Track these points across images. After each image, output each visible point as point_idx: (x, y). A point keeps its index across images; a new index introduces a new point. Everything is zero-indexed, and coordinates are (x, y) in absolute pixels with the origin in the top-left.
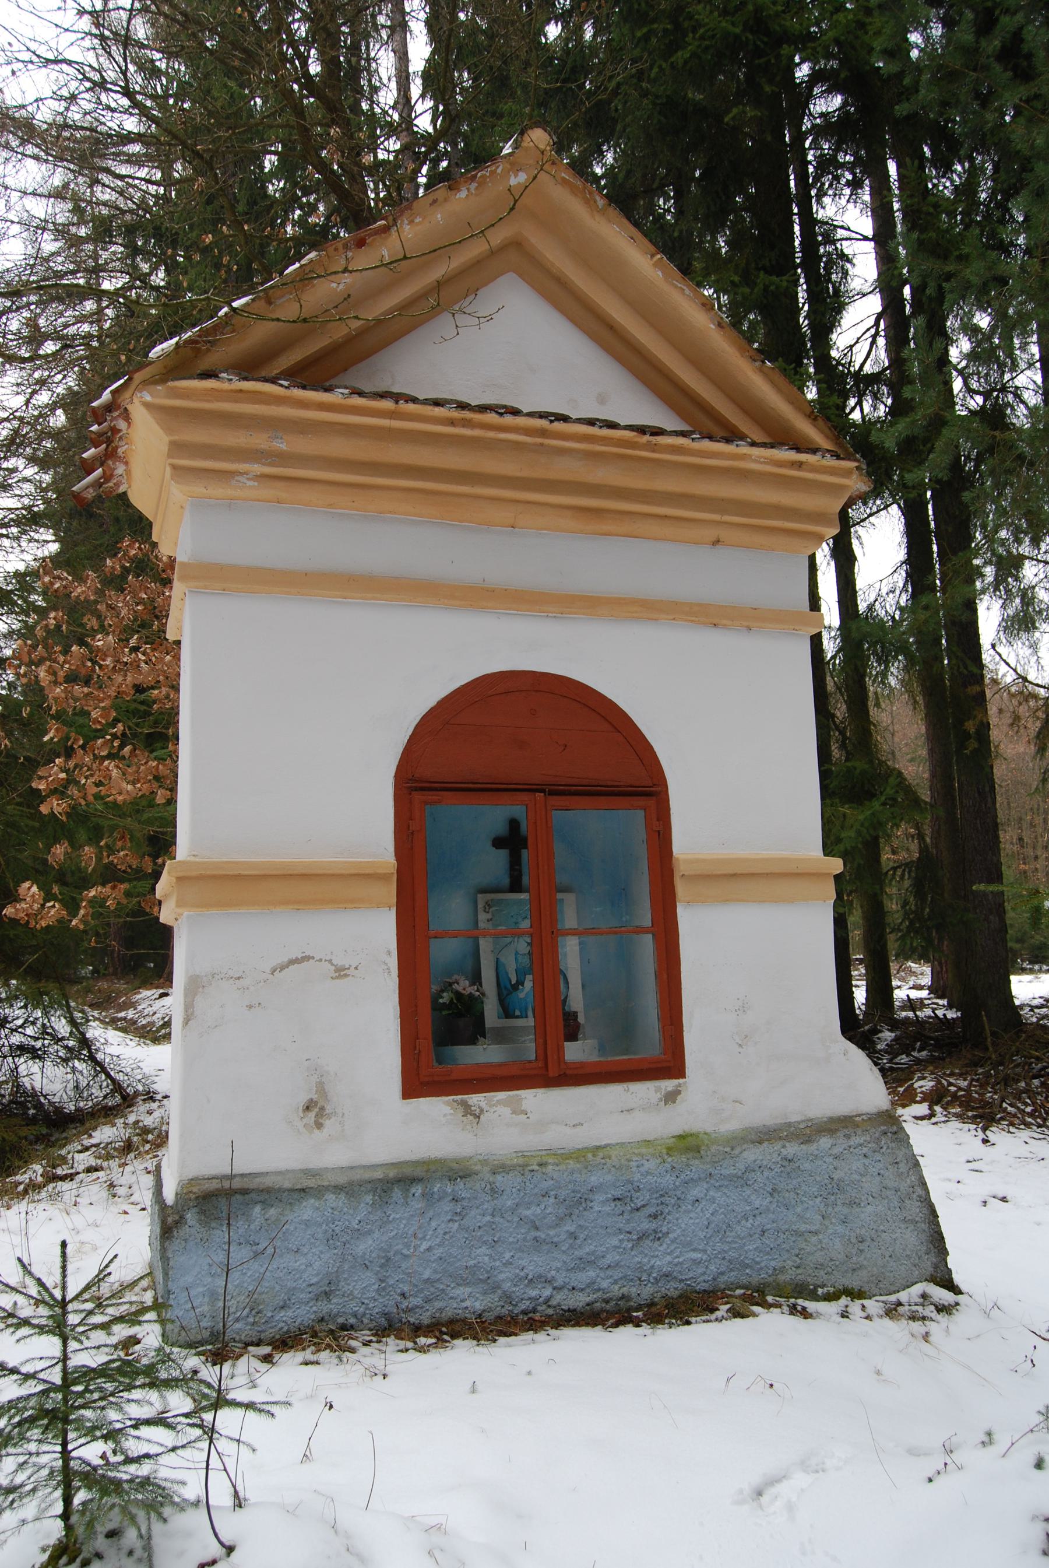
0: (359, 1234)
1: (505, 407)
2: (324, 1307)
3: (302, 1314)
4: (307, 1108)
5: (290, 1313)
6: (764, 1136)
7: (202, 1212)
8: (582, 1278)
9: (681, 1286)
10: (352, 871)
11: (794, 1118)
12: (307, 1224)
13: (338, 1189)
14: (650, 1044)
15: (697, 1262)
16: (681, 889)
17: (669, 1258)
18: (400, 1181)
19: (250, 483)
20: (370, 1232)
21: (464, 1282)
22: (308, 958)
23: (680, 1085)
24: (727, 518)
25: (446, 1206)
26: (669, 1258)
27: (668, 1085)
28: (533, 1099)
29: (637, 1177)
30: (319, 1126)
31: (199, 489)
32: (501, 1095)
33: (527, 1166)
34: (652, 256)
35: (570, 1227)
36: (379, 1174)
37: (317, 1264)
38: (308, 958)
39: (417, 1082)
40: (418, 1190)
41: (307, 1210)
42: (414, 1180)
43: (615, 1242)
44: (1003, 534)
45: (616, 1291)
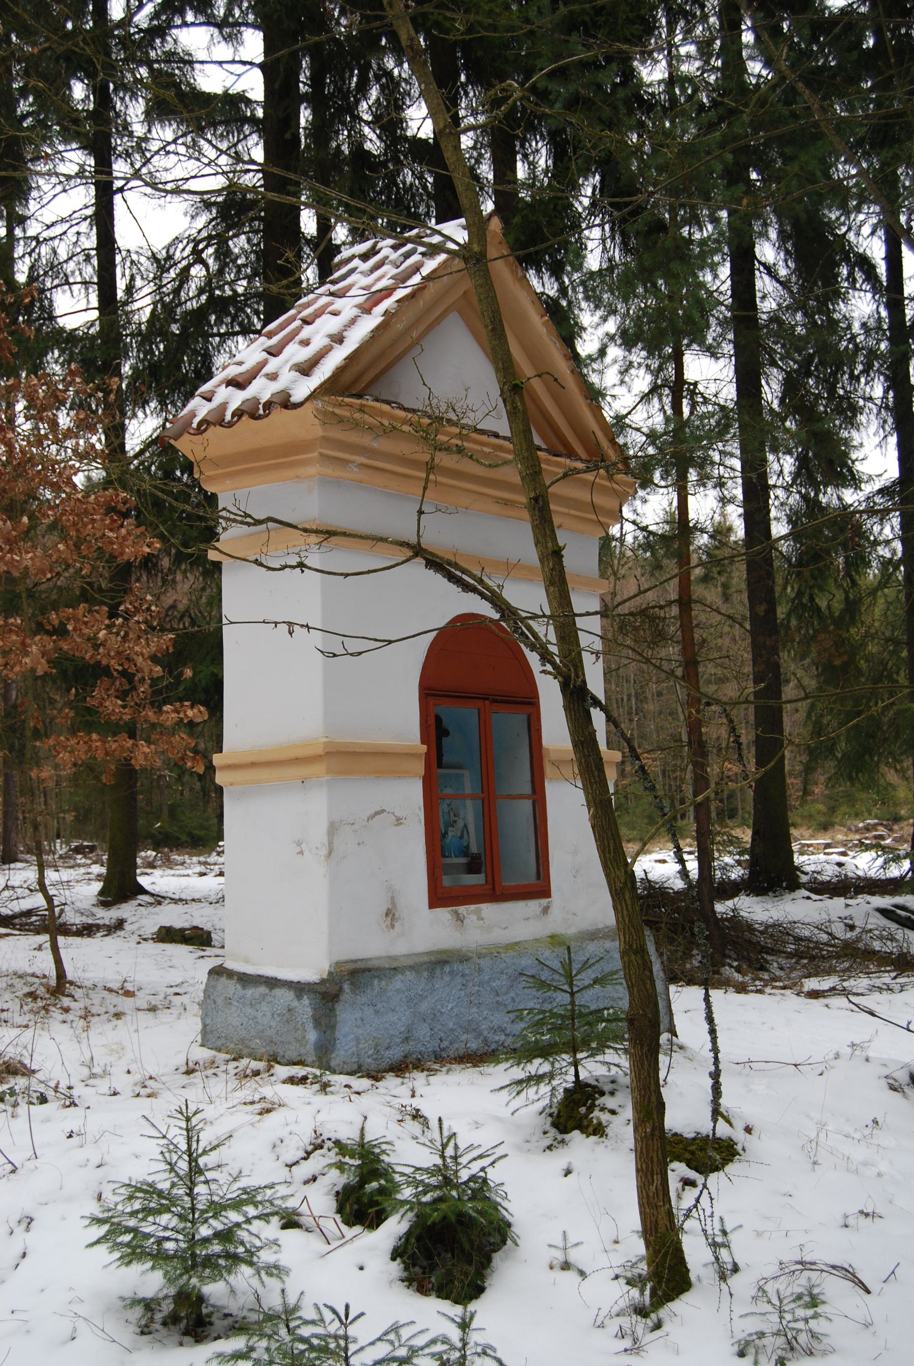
0: (422, 997)
2: (407, 1048)
3: (395, 1054)
4: (387, 915)
7: (352, 984)
11: (601, 926)
12: (398, 991)
13: (411, 968)
16: (549, 770)
18: (439, 963)
19: (355, 469)
20: (426, 997)
21: (467, 1032)
22: (383, 811)
24: (572, 512)
25: (459, 980)
27: (544, 902)
28: (487, 909)
30: (393, 926)
31: (329, 471)
32: (473, 907)
33: (493, 952)
34: (542, 316)
35: (512, 994)
36: (426, 959)
38: (383, 811)
39: (439, 897)
40: (447, 969)
41: (398, 983)
42: (446, 962)
44: (648, 554)
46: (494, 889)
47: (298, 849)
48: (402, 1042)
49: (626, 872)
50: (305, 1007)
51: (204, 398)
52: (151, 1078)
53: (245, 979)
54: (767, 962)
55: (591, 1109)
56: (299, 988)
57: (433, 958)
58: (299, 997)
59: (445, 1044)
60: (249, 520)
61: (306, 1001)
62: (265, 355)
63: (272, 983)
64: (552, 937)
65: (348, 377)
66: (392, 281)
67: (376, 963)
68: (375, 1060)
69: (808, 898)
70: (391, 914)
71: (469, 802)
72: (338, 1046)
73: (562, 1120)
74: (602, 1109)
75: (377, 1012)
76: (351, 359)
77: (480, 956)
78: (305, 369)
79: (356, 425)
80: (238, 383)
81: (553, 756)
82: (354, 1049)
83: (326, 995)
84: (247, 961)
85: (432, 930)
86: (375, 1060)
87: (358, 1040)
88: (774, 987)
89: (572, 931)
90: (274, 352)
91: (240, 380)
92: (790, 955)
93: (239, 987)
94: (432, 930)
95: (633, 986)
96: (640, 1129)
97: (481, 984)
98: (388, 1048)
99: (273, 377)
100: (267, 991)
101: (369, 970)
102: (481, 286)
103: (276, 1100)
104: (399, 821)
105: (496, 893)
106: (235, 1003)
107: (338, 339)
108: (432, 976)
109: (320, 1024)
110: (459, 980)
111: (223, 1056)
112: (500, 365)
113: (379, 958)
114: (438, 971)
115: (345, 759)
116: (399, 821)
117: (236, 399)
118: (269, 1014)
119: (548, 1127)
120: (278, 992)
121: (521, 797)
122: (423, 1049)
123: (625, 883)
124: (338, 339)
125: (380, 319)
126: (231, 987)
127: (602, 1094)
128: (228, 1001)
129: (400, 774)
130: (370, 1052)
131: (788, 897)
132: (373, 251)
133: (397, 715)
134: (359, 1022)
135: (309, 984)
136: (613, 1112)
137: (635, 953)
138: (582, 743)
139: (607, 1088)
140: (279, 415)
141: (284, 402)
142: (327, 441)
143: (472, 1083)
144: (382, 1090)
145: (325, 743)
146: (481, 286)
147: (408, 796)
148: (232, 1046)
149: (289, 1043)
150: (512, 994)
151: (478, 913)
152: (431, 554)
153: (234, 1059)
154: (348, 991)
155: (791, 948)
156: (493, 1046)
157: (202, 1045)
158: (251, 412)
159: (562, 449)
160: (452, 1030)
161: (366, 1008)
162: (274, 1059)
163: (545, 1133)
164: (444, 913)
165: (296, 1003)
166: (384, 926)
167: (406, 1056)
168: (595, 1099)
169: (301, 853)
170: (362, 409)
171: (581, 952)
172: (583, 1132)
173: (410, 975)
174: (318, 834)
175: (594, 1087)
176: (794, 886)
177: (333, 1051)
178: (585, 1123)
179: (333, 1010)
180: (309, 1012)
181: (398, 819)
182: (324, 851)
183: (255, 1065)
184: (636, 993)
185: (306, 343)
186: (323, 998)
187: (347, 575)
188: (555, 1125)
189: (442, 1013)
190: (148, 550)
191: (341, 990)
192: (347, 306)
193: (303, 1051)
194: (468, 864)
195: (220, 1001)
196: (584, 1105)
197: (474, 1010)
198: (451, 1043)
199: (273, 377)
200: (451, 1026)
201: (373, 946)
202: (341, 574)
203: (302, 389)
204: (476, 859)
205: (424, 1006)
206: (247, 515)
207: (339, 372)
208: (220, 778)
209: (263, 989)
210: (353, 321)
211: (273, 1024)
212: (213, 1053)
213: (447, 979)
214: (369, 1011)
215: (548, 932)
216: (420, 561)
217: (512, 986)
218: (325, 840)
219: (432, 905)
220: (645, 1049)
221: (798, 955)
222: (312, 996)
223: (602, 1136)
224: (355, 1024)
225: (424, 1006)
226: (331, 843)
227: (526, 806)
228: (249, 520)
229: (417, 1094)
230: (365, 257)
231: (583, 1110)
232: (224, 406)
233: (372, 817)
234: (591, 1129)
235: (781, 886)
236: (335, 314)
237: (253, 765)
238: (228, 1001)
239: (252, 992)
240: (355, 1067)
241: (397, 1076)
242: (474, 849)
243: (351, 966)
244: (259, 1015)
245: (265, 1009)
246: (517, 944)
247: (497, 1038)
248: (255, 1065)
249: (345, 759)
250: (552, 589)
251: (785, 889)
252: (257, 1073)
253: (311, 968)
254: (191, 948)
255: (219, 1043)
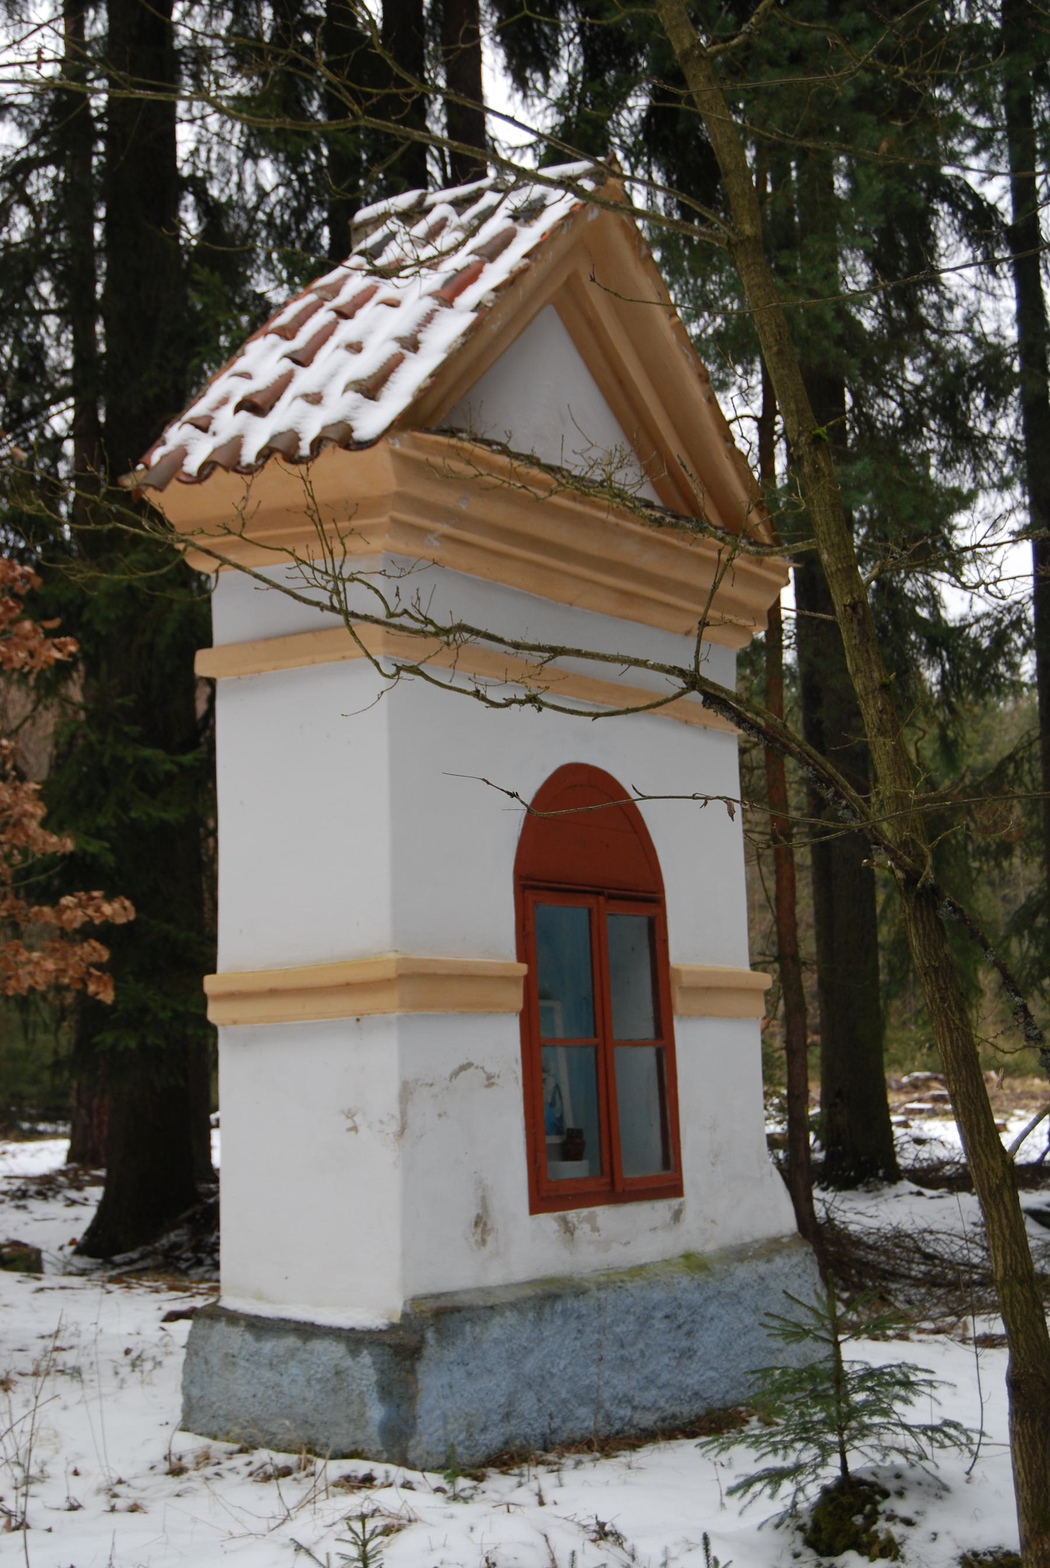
0: (528, 1351)
1: (207, 477)
2: (509, 1429)
3: (492, 1439)
4: (476, 1224)
5: (488, 1436)
6: (740, 1254)
7: (438, 1331)
8: (651, 1395)
9: (704, 1404)
10: (341, 977)
11: (748, 1239)
12: (496, 1342)
13: (513, 1306)
14: (640, 1160)
15: (713, 1380)
16: (679, 1002)
17: (697, 1377)
18: (548, 1297)
19: (436, 544)
20: (532, 1351)
22: (469, 1065)
23: (681, 1204)
25: (573, 1324)
26: (697, 1377)
27: (675, 1202)
28: (604, 1214)
29: (679, 1295)
30: (484, 1242)
31: (400, 545)
32: (585, 1212)
33: (613, 1280)
35: (641, 1345)
36: (529, 1292)
37: (504, 1383)
38: (469, 1065)
39: (544, 1197)
40: (559, 1307)
41: (496, 1329)
42: (554, 1297)
43: (665, 1360)
45: (670, 1410)
46: (612, 1183)
47: (349, 1124)
48: (501, 1421)
49: (1004, 1162)
50: (364, 1370)
51: (197, 427)
52: (120, 1482)
53: (259, 1326)
54: (889, 1292)
55: (872, 1518)
56: (354, 1339)
57: (539, 1291)
58: (354, 1353)
59: (557, 1423)
60: (430, 628)
61: (366, 1358)
62: (288, 364)
63: (307, 1331)
64: (687, 1256)
65: (430, 403)
66: (473, 258)
67: (465, 1300)
68: (467, 1448)
69: (920, 1194)
70: (481, 1223)
71: (561, 1052)
72: (420, 1427)
73: (824, 1536)
74: (891, 1518)
75: (469, 1374)
76: (438, 375)
77: (600, 1287)
78: (371, 388)
79: (449, 479)
80: (256, 406)
81: (686, 981)
82: (441, 1432)
83: (402, 1348)
84: (260, 1297)
85: (533, 1247)
86: (467, 1448)
87: (445, 1418)
88: (921, 1331)
89: (710, 1248)
90: (302, 359)
91: (258, 400)
92: (917, 1283)
93: (249, 1337)
94: (533, 1247)
95: (1017, 1331)
96: (1034, 1545)
97: (602, 1330)
98: (484, 1430)
99: (315, 399)
100: (299, 1343)
101: (457, 1309)
102: (759, 286)
103: (404, 1513)
104: (490, 1081)
105: (614, 1189)
106: (243, 1363)
107: (411, 344)
108: (539, 1318)
109: (390, 1393)
110: (573, 1324)
111: (219, 1447)
112: (793, 406)
113: (467, 1291)
114: (547, 1310)
115: (425, 986)
116: (490, 1081)
117: (258, 433)
118: (301, 1380)
119: (799, 1546)
120: (318, 1345)
121: (643, 1043)
122: (528, 1430)
123: (1004, 1179)
124: (411, 344)
125: (470, 318)
126: (237, 1338)
127: (886, 1495)
128: (230, 1360)
129: (489, 1008)
130: (462, 1437)
131: (889, 1191)
132: (419, 211)
133: (484, 921)
134: (447, 1391)
135: (370, 1332)
136: (908, 1522)
137: (1021, 1283)
138: (936, 970)
139: (891, 1485)
140: (333, 458)
141: (341, 437)
142: (403, 499)
143: (625, 1483)
144: (490, 1494)
145: (398, 960)
146: (759, 286)
147: (499, 1041)
148: (237, 1430)
149: (337, 1424)
150: (641, 1345)
151: (591, 1219)
152: (713, 685)
153: (241, 1451)
154: (432, 1342)
155: (918, 1269)
156: (618, 1425)
157: (184, 1429)
158: (283, 449)
159: (686, 512)
160: (564, 1401)
161: (455, 1368)
162: (312, 1450)
163: (796, 1556)
164: (548, 1221)
165: (349, 1362)
166: (472, 1240)
167: (506, 1443)
168: (875, 1504)
169: (354, 1129)
170: (457, 453)
171: (728, 1280)
172: (862, 1554)
173: (511, 1317)
174: (384, 1099)
175: (872, 1485)
176: (894, 1175)
177: (409, 1436)
178: (865, 1538)
179: (412, 1371)
180: (371, 1376)
181: (489, 1077)
182: (394, 1127)
183: (283, 1459)
184: (1022, 1342)
185: (355, 348)
186: (396, 1353)
187: (596, 716)
188: (809, 1543)
189: (552, 1375)
190: (58, 655)
191: (423, 1340)
192: (416, 292)
193: (360, 1436)
194: (564, 1145)
195: (215, 1360)
196: (860, 1512)
197: (593, 1369)
198: (564, 1421)
199: (315, 399)
200: (564, 1395)
201: (461, 1273)
202: (589, 714)
203: (372, 419)
204: (593, 1139)
205: (530, 1365)
206: (428, 621)
207: (422, 396)
208: (213, 1014)
209: (291, 1341)
210: (429, 318)
211: (310, 1395)
212: (204, 1441)
213: (559, 1322)
214: (459, 1372)
215: (679, 1249)
216: (696, 696)
217: (640, 1332)
218: (396, 1110)
219: (535, 1208)
220: (1039, 1425)
221: (931, 1281)
222: (378, 1350)
223: (895, 1559)
224: (444, 1395)
225: (530, 1365)
226: (403, 1114)
227: (647, 1056)
228: (430, 628)
229: (548, 1499)
230: (409, 216)
231: (858, 1520)
232: (236, 443)
233: (455, 1074)
234: (876, 1549)
235: (876, 1176)
236: (394, 304)
237: (273, 993)
238: (230, 1360)
239: (269, 1346)
240: (442, 1460)
241: (504, 1473)
242: (569, 1123)
243: (433, 1304)
244: (285, 1381)
245: (294, 1371)
246: (642, 1267)
247: (622, 1412)
248: (283, 1459)
249: (425, 986)
250: (93, 681)
251: (882, 1179)
252: (285, 1472)
253: (374, 1308)
254: (17, 1275)
255: (214, 1426)
